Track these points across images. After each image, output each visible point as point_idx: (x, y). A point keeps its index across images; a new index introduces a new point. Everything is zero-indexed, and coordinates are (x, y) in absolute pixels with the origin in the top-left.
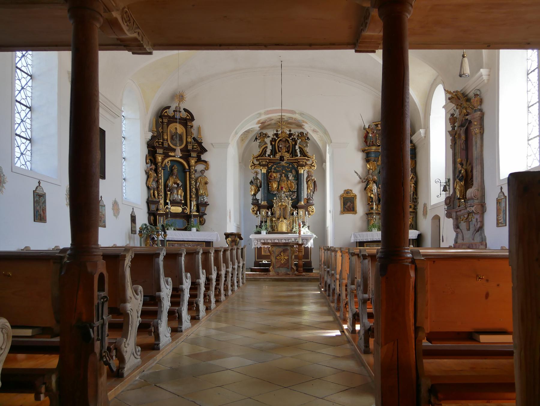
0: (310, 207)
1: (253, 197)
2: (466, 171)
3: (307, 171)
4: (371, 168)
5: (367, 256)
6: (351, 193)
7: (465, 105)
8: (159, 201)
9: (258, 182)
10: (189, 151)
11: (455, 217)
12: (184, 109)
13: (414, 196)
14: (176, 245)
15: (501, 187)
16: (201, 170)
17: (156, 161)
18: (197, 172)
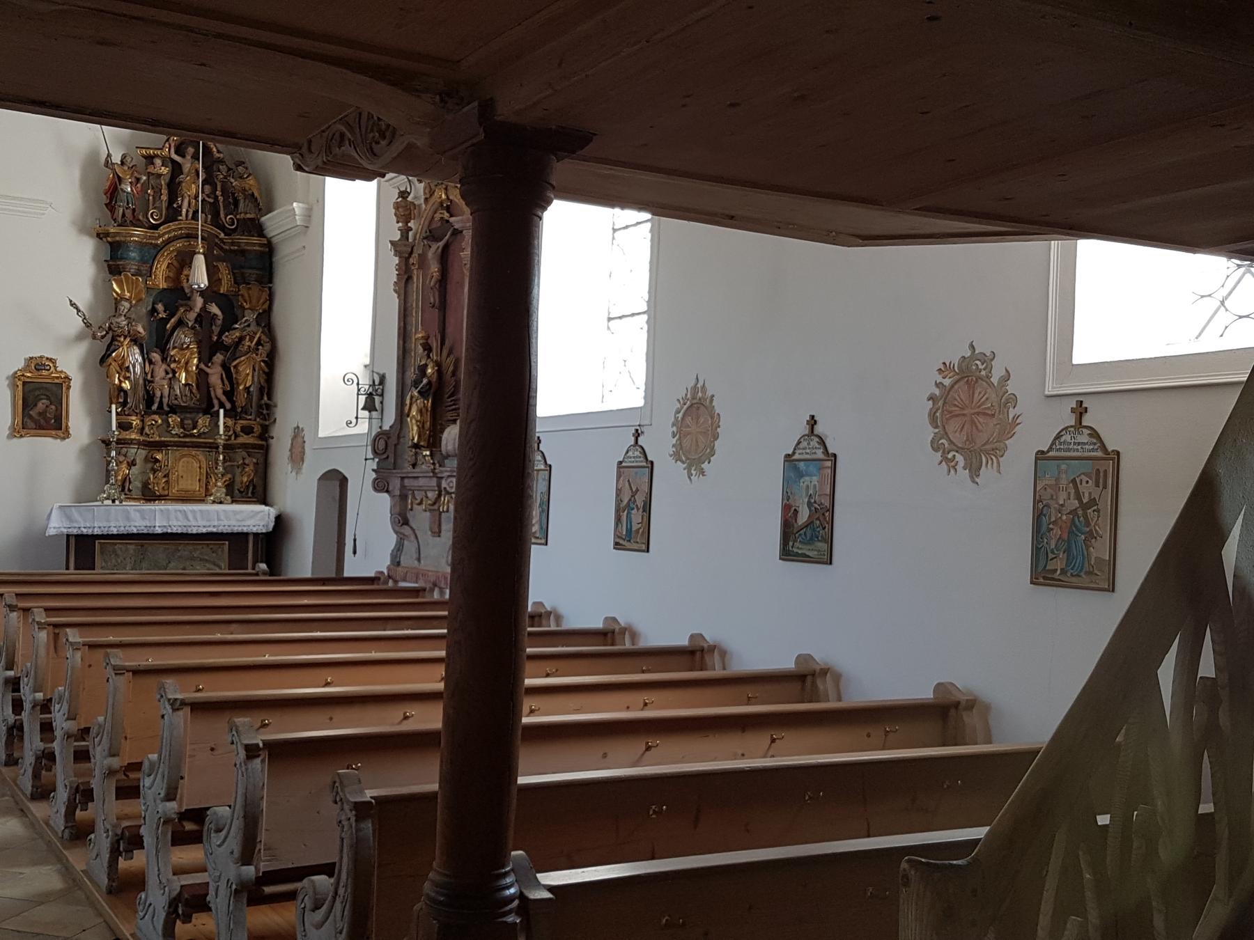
2: (440, 372)
4: (127, 295)
6: (52, 369)
11: (397, 493)
12: (218, 886)
13: (262, 399)
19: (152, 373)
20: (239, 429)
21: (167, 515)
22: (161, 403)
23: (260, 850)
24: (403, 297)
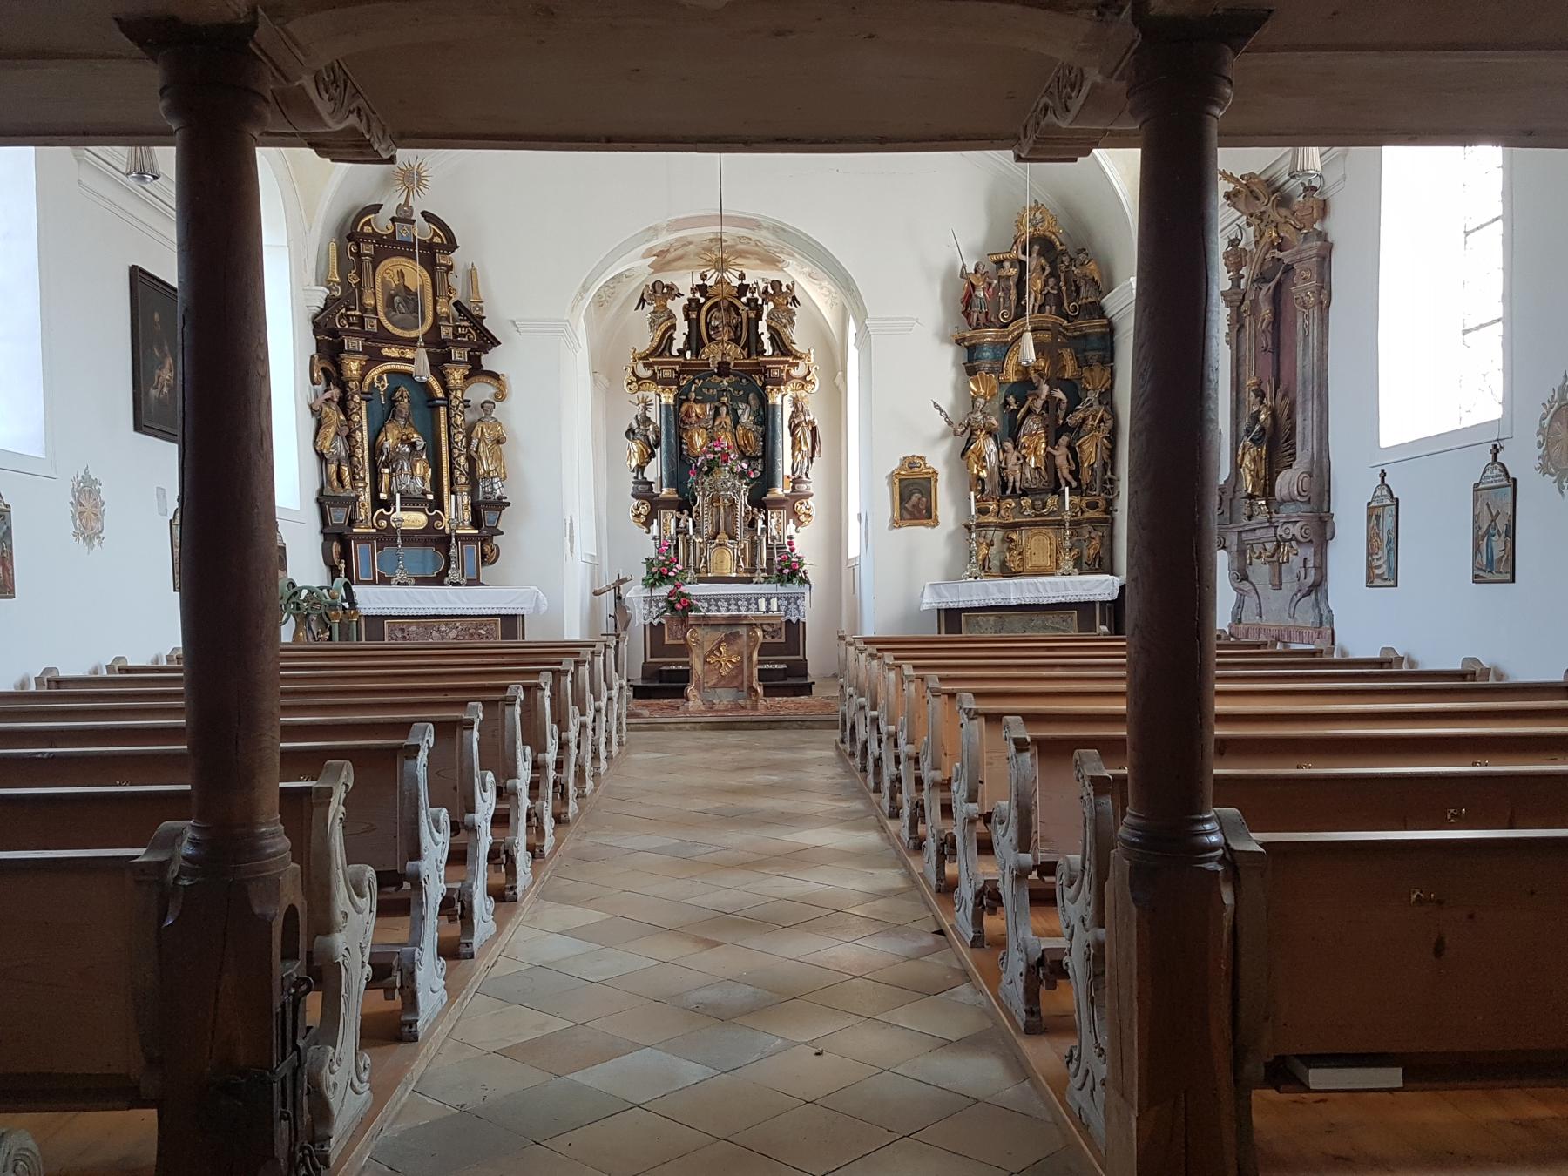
0: (802, 503)
1: (635, 475)
2: (1274, 414)
3: (791, 396)
6: (923, 466)
7: (1275, 216)
8: (357, 497)
9: (651, 430)
10: (443, 344)
11: (1235, 548)
12: (424, 214)
14: (413, 628)
15: (1383, 471)
16: (485, 402)
17: (342, 375)
18: (469, 406)
20: (1084, 505)
21: (1020, 587)
22: (1014, 487)
23: (1037, 840)
24: (1235, 347)
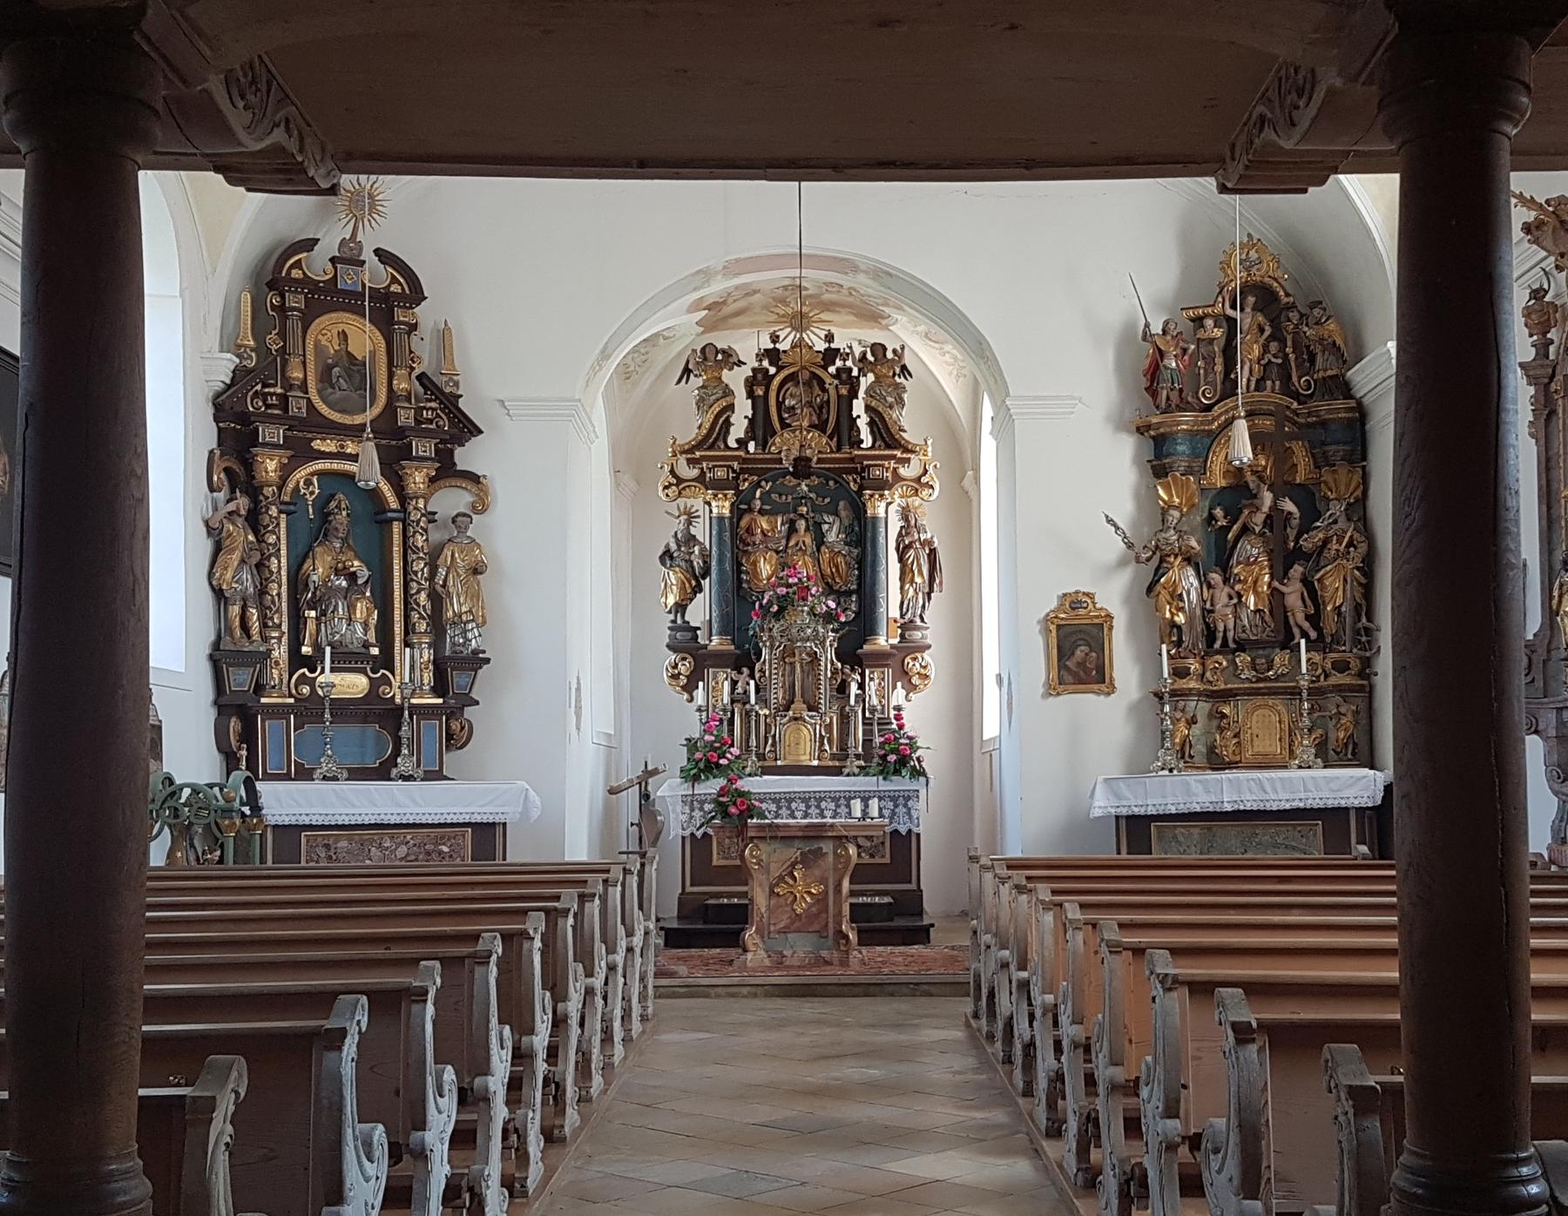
0: (915, 659)
1: (672, 617)
3: (899, 505)
5: (1254, 1031)
6: (1091, 606)
9: (697, 552)
10: (401, 433)
11: (1553, 733)
12: (378, 252)
13: (1360, 620)
14: (343, 844)
17: (253, 477)
19: (1212, 600)
